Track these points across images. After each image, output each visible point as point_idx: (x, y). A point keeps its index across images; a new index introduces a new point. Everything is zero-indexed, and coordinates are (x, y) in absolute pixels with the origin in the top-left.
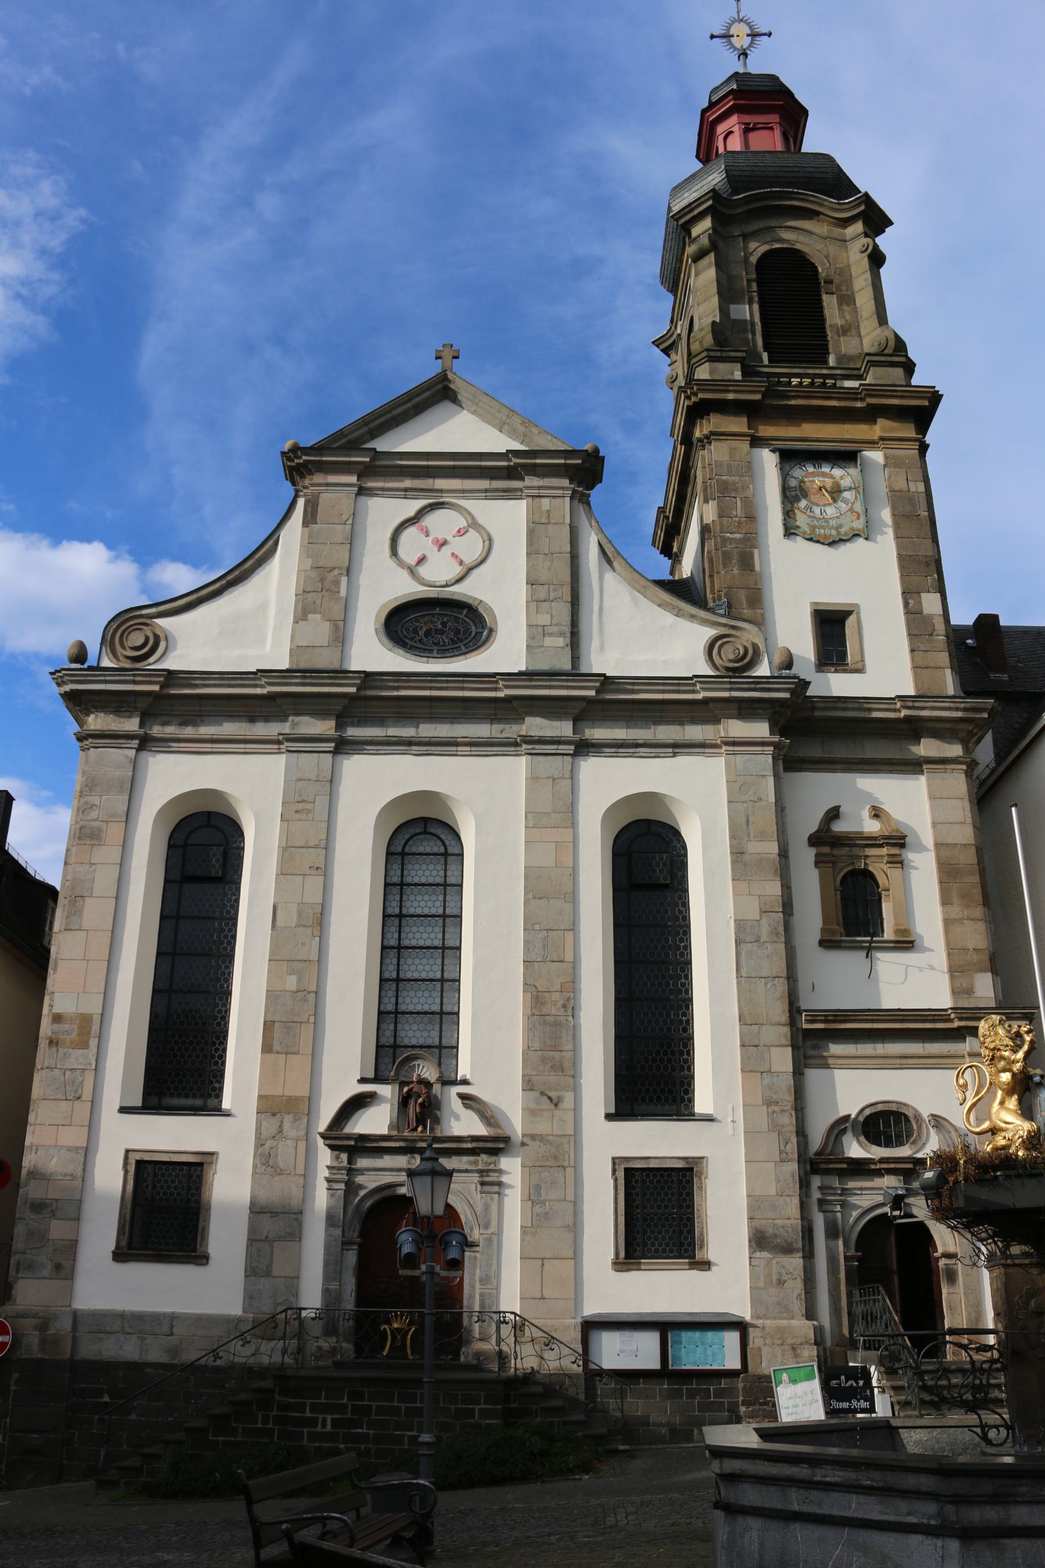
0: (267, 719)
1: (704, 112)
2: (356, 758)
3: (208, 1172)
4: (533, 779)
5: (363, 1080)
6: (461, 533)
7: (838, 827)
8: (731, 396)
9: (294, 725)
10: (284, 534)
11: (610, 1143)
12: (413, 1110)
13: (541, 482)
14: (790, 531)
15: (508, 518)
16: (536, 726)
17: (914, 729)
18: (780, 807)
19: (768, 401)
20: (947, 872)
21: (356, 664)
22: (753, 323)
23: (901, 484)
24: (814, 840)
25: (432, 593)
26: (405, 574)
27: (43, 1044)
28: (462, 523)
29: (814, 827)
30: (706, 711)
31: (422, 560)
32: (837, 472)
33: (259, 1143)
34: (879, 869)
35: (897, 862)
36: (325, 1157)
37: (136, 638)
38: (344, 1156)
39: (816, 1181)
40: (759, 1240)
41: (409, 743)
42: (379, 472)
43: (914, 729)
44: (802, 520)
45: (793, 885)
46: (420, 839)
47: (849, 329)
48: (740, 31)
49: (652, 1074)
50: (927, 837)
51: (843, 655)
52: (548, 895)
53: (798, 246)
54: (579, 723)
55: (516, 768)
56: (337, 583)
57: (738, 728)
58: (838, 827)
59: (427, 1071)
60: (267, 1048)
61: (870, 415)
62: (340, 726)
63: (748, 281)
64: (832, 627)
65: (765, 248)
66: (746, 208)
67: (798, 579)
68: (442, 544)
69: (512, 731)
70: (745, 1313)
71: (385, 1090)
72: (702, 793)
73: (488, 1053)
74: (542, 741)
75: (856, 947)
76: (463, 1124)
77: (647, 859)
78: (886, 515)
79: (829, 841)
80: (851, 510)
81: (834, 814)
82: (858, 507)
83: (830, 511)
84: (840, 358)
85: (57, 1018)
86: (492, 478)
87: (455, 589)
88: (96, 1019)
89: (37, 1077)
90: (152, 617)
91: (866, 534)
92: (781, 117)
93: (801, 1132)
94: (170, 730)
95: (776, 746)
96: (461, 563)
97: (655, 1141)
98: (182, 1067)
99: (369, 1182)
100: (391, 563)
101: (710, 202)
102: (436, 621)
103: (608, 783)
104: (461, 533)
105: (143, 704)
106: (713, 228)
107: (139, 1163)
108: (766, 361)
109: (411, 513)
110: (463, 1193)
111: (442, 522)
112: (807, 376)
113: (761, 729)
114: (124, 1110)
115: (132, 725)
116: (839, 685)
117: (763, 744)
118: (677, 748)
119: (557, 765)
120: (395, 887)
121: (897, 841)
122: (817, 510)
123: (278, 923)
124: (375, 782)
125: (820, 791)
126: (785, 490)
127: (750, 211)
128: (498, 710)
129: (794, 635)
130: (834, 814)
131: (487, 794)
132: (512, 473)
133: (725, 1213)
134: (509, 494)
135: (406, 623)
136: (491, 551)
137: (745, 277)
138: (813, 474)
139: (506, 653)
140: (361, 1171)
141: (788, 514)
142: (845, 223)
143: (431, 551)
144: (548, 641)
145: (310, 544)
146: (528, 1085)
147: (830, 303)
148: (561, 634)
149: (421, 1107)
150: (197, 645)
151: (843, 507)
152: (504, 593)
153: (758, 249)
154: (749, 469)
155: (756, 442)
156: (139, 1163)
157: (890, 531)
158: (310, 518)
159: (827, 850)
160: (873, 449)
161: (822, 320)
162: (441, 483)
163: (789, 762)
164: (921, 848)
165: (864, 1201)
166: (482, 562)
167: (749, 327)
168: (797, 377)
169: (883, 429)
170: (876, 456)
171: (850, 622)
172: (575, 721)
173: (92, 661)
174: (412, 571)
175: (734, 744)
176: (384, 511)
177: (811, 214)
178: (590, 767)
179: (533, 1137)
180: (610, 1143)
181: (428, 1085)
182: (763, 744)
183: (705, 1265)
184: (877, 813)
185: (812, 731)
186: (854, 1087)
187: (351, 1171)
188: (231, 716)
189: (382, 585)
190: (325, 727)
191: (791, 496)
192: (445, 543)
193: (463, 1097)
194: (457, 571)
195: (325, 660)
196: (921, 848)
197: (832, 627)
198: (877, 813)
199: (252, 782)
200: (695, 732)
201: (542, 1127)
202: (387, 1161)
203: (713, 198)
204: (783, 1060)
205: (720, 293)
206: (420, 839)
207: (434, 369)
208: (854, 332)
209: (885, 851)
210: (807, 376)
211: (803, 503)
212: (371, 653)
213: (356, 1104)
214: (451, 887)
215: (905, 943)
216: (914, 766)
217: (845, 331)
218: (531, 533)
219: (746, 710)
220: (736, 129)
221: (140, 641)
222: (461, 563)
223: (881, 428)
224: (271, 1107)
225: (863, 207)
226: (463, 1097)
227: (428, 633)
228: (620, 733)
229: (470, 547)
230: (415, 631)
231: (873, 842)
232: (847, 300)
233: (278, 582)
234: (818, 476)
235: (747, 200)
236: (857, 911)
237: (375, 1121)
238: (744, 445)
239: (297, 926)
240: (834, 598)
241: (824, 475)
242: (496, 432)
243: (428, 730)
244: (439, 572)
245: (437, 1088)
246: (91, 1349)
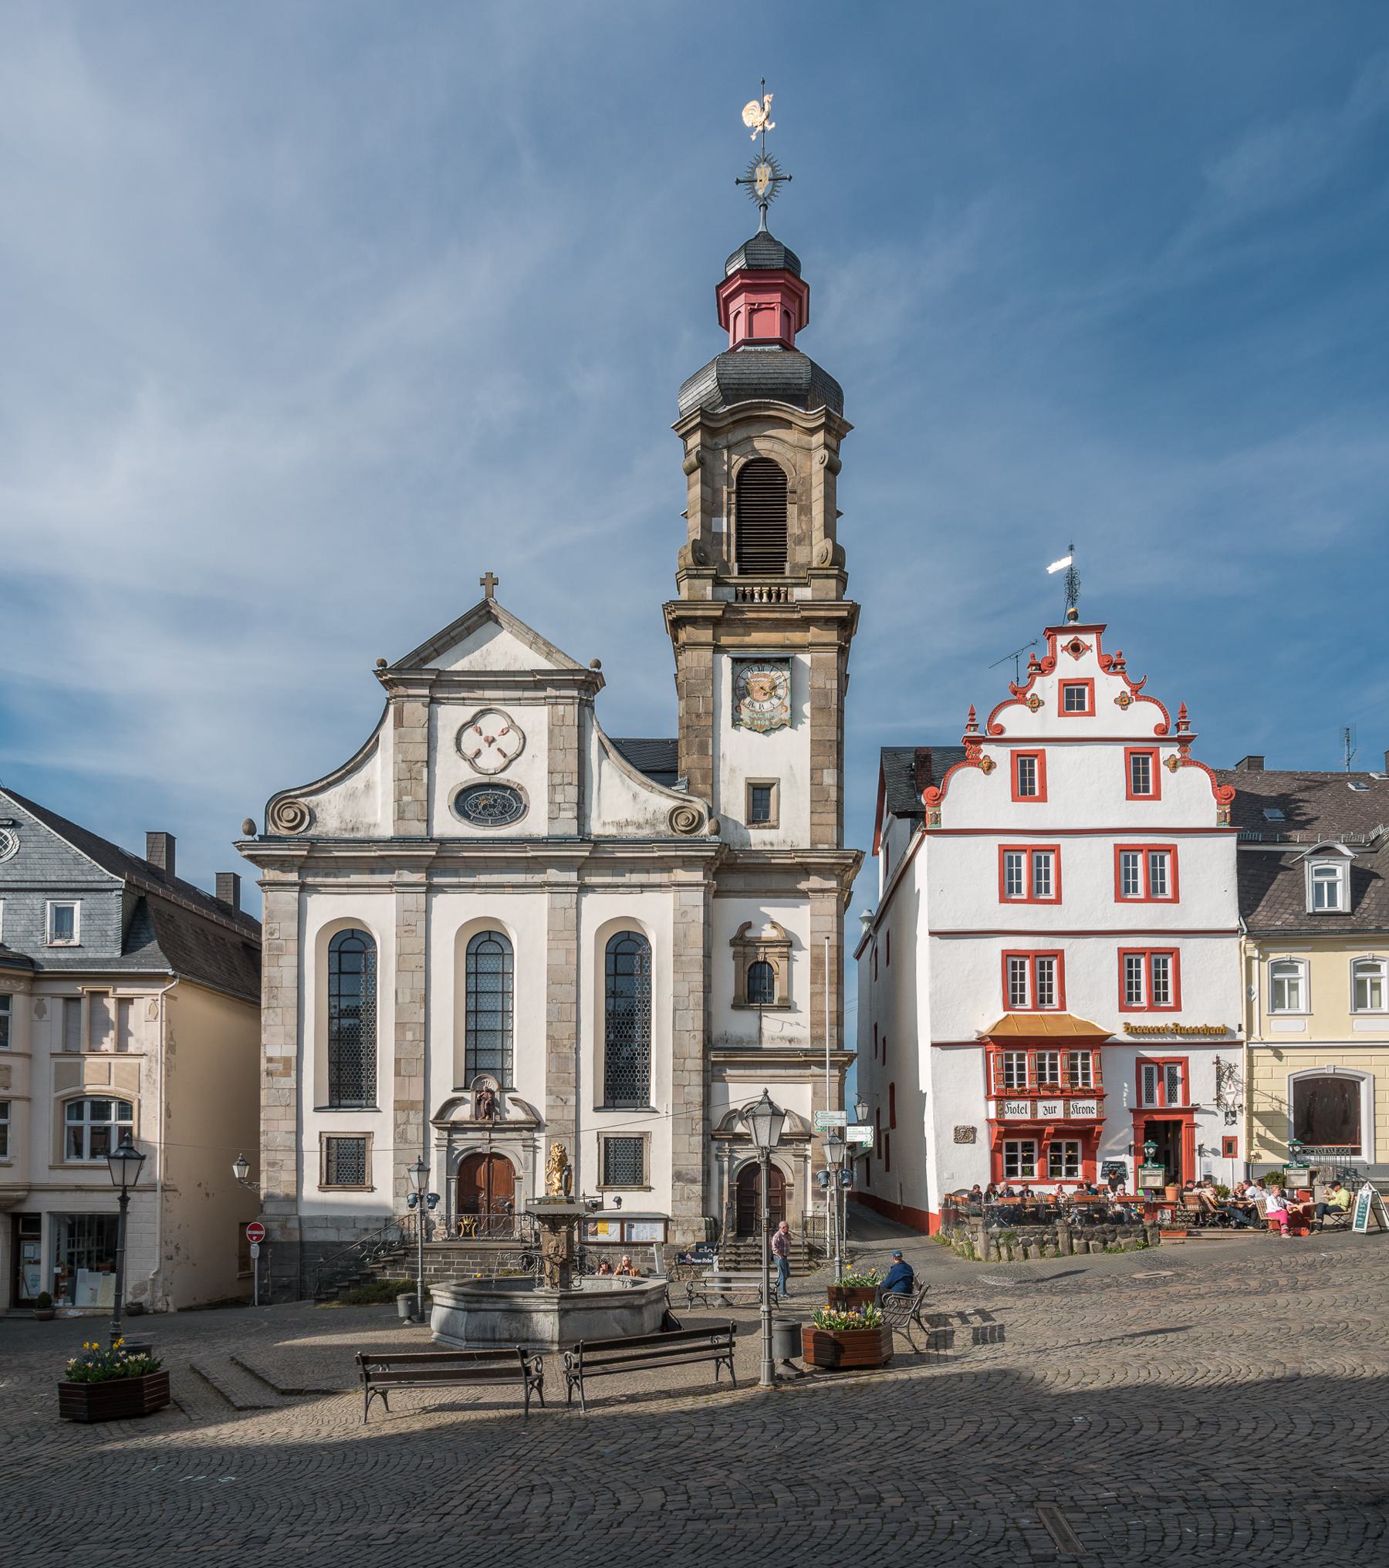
0: (382, 872)
1: (718, 288)
2: (440, 896)
3: (369, 1143)
4: (552, 909)
5: (455, 1090)
6: (504, 733)
7: (749, 934)
8: (699, 613)
9: (399, 875)
10: (382, 733)
11: (597, 1124)
12: (483, 1107)
13: (557, 693)
14: (736, 722)
15: (535, 718)
16: (553, 875)
17: (806, 870)
18: (708, 924)
19: (727, 616)
20: (817, 962)
21: (438, 831)
22: (729, 535)
23: (820, 683)
24: (733, 943)
25: (485, 780)
26: (466, 765)
27: (263, 1075)
28: (504, 724)
29: (734, 934)
30: (664, 865)
31: (478, 753)
32: (774, 674)
33: (396, 1126)
34: (780, 966)
35: (789, 958)
36: (434, 1133)
37: (289, 814)
38: (445, 1134)
39: (715, 1144)
40: (678, 1176)
41: (474, 886)
42: (443, 687)
43: (806, 870)
44: (745, 714)
45: (713, 973)
46: (486, 948)
47: (804, 539)
48: (763, 173)
49: (623, 1084)
50: (806, 942)
51: (767, 815)
52: (562, 982)
53: (772, 456)
54: (583, 872)
55: (541, 902)
56: (420, 772)
57: (681, 875)
58: (749, 934)
59: (492, 1084)
60: (397, 1074)
61: (805, 623)
62: (429, 876)
63: (729, 493)
64: (760, 795)
65: (743, 461)
66: (731, 420)
67: (743, 755)
68: (491, 741)
69: (538, 878)
70: (668, 1212)
71: (469, 1096)
72: (664, 914)
73: (529, 1077)
74: (557, 885)
75: (752, 1009)
76: (515, 1114)
77: (625, 953)
78: (806, 708)
79: (743, 942)
80: (782, 704)
81: (748, 926)
82: (787, 702)
83: (767, 706)
84: (792, 570)
85: (270, 1060)
86: (525, 689)
87: (501, 775)
88: (294, 1061)
89: (263, 1093)
90: (296, 797)
91: (793, 721)
92: (783, 294)
93: (706, 1119)
94: (319, 880)
95: (705, 886)
96: (505, 756)
97: (623, 1122)
98: (350, 1082)
99: (460, 1146)
100: (456, 757)
101: (698, 420)
102: (490, 799)
103: (601, 910)
104: (504, 733)
105: (297, 862)
106: (702, 444)
107: (328, 1139)
108: (736, 574)
109: (469, 718)
110: (511, 1148)
111: (492, 724)
112: (765, 585)
113: (698, 876)
114: (317, 1109)
115: (293, 877)
116: (758, 838)
117: (698, 885)
118: (643, 887)
119: (569, 900)
120: (473, 974)
121: (789, 943)
122: (757, 705)
123: (400, 1000)
124: (455, 911)
125: (735, 910)
126: (735, 689)
127: (734, 422)
128: (527, 861)
129: (734, 804)
130: (748, 926)
131: (526, 916)
132: (538, 686)
133: (660, 1163)
134: (534, 702)
135: (467, 801)
136: (525, 745)
137: (726, 494)
138: (757, 676)
139: (536, 822)
140: (454, 1141)
141: (736, 709)
142: (812, 431)
143: (484, 746)
144: (563, 814)
145: (399, 742)
146: (550, 1092)
147: (792, 510)
148: (571, 809)
149: (489, 1107)
150: (333, 813)
151: (775, 701)
152: (532, 776)
153: (739, 461)
154: (713, 673)
155: (718, 649)
156: (328, 1139)
157: (808, 721)
158: (399, 722)
159: (741, 949)
160: (803, 652)
161: (783, 527)
162: (489, 694)
163: (716, 893)
164: (801, 948)
165: (742, 1156)
166: (518, 755)
167: (725, 539)
168: (759, 586)
169: (814, 636)
170: (805, 658)
171: (773, 790)
172: (579, 870)
173: (260, 831)
174: (472, 762)
175: (679, 885)
176: (451, 716)
177: (788, 424)
178: (589, 900)
179: (551, 1121)
180: (597, 1124)
181: (492, 1093)
182: (698, 885)
183: (650, 1189)
184: (774, 925)
185: (732, 871)
186: (740, 1092)
187: (450, 1141)
188: (359, 870)
189: (452, 774)
190: (419, 877)
191: (740, 692)
192: (494, 740)
193: (512, 1099)
194: (502, 761)
195: (417, 829)
196: (801, 948)
197: (760, 795)
198: (774, 925)
199: (378, 911)
200: (655, 878)
201: (557, 1114)
202: (470, 1135)
203: (701, 415)
204: (697, 1079)
205: (703, 511)
206: (486, 948)
207: (480, 595)
208: (807, 541)
209: (777, 950)
210: (765, 585)
211: (748, 700)
212: (447, 824)
213: (451, 1104)
214: (505, 975)
215: (787, 1006)
216: (804, 895)
217: (799, 541)
218: (551, 732)
219: (687, 863)
220: (742, 309)
221: (292, 816)
222: (505, 756)
223: (813, 634)
224: (400, 1106)
225: (823, 420)
226: (512, 1099)
227: (485, 807)
228: (608, 880)
229: (510, 744)
230: (476, 806)
231: (771, 943)
232: (806, 510)
233: (381, 770)
234: (759, 678)
235: (732, 412)
236: (757, 987)
237: (463, 1113)
238: (707, 654)
239: (300, 1219)
240: (762, 773)
241: (765, 676)
242: (527, 648)
243: (484, 878)
244: (490, 761)
245: (497, 1095)
246: (311, 1236)
